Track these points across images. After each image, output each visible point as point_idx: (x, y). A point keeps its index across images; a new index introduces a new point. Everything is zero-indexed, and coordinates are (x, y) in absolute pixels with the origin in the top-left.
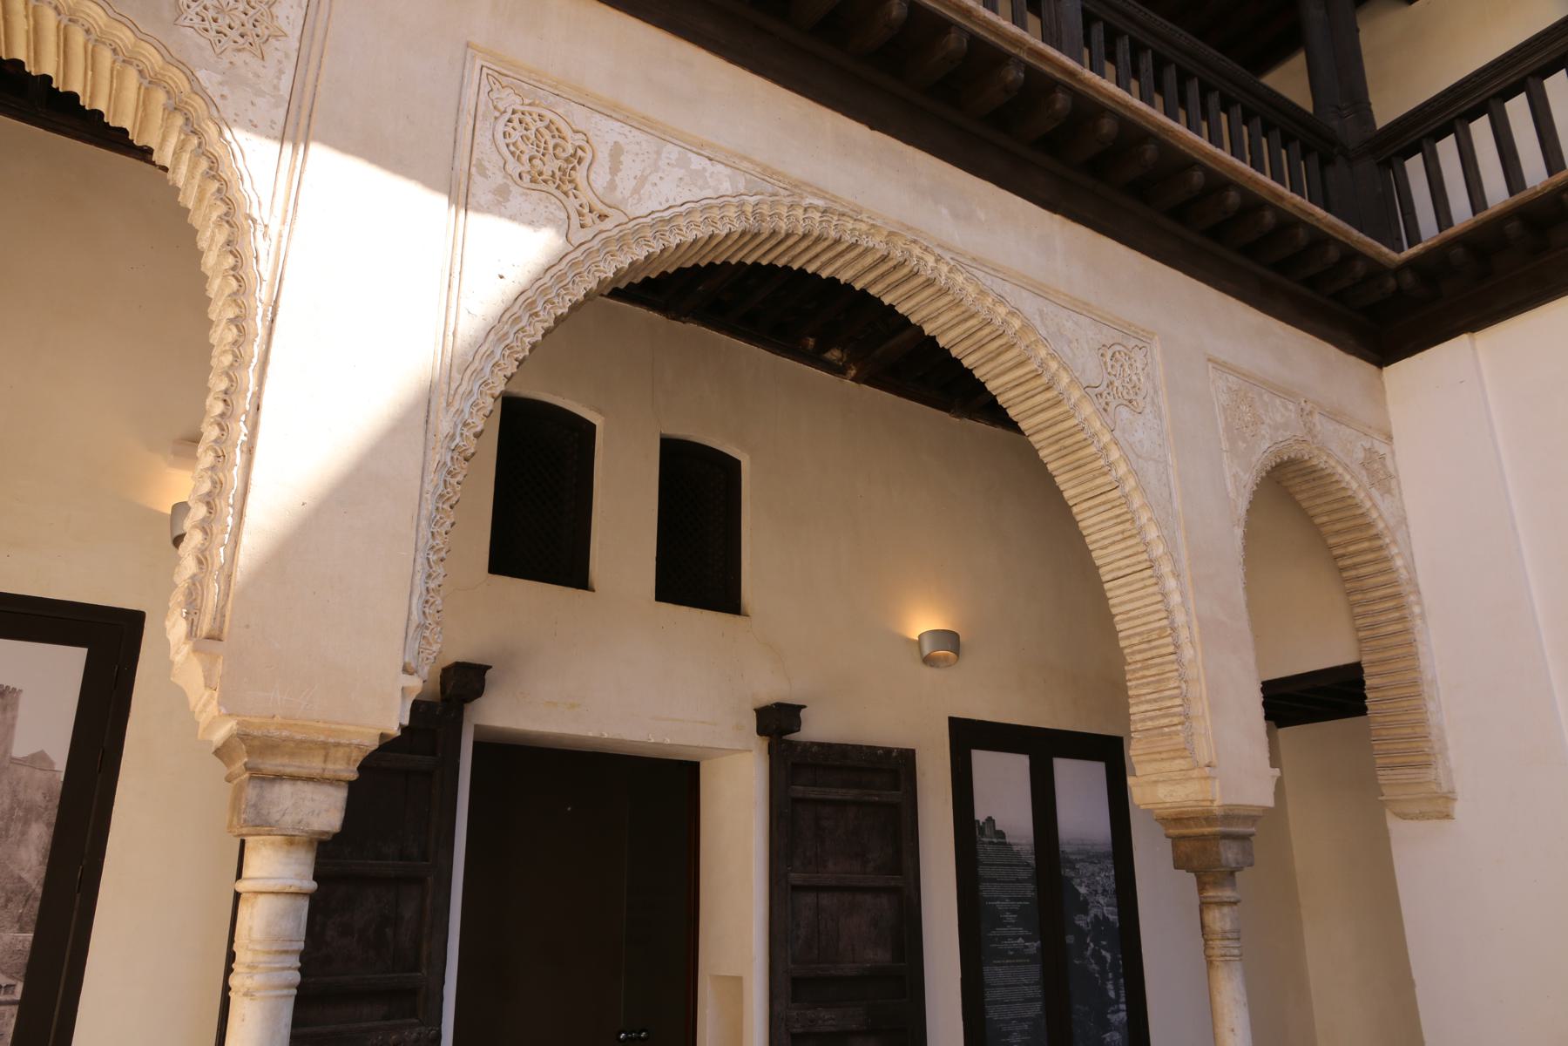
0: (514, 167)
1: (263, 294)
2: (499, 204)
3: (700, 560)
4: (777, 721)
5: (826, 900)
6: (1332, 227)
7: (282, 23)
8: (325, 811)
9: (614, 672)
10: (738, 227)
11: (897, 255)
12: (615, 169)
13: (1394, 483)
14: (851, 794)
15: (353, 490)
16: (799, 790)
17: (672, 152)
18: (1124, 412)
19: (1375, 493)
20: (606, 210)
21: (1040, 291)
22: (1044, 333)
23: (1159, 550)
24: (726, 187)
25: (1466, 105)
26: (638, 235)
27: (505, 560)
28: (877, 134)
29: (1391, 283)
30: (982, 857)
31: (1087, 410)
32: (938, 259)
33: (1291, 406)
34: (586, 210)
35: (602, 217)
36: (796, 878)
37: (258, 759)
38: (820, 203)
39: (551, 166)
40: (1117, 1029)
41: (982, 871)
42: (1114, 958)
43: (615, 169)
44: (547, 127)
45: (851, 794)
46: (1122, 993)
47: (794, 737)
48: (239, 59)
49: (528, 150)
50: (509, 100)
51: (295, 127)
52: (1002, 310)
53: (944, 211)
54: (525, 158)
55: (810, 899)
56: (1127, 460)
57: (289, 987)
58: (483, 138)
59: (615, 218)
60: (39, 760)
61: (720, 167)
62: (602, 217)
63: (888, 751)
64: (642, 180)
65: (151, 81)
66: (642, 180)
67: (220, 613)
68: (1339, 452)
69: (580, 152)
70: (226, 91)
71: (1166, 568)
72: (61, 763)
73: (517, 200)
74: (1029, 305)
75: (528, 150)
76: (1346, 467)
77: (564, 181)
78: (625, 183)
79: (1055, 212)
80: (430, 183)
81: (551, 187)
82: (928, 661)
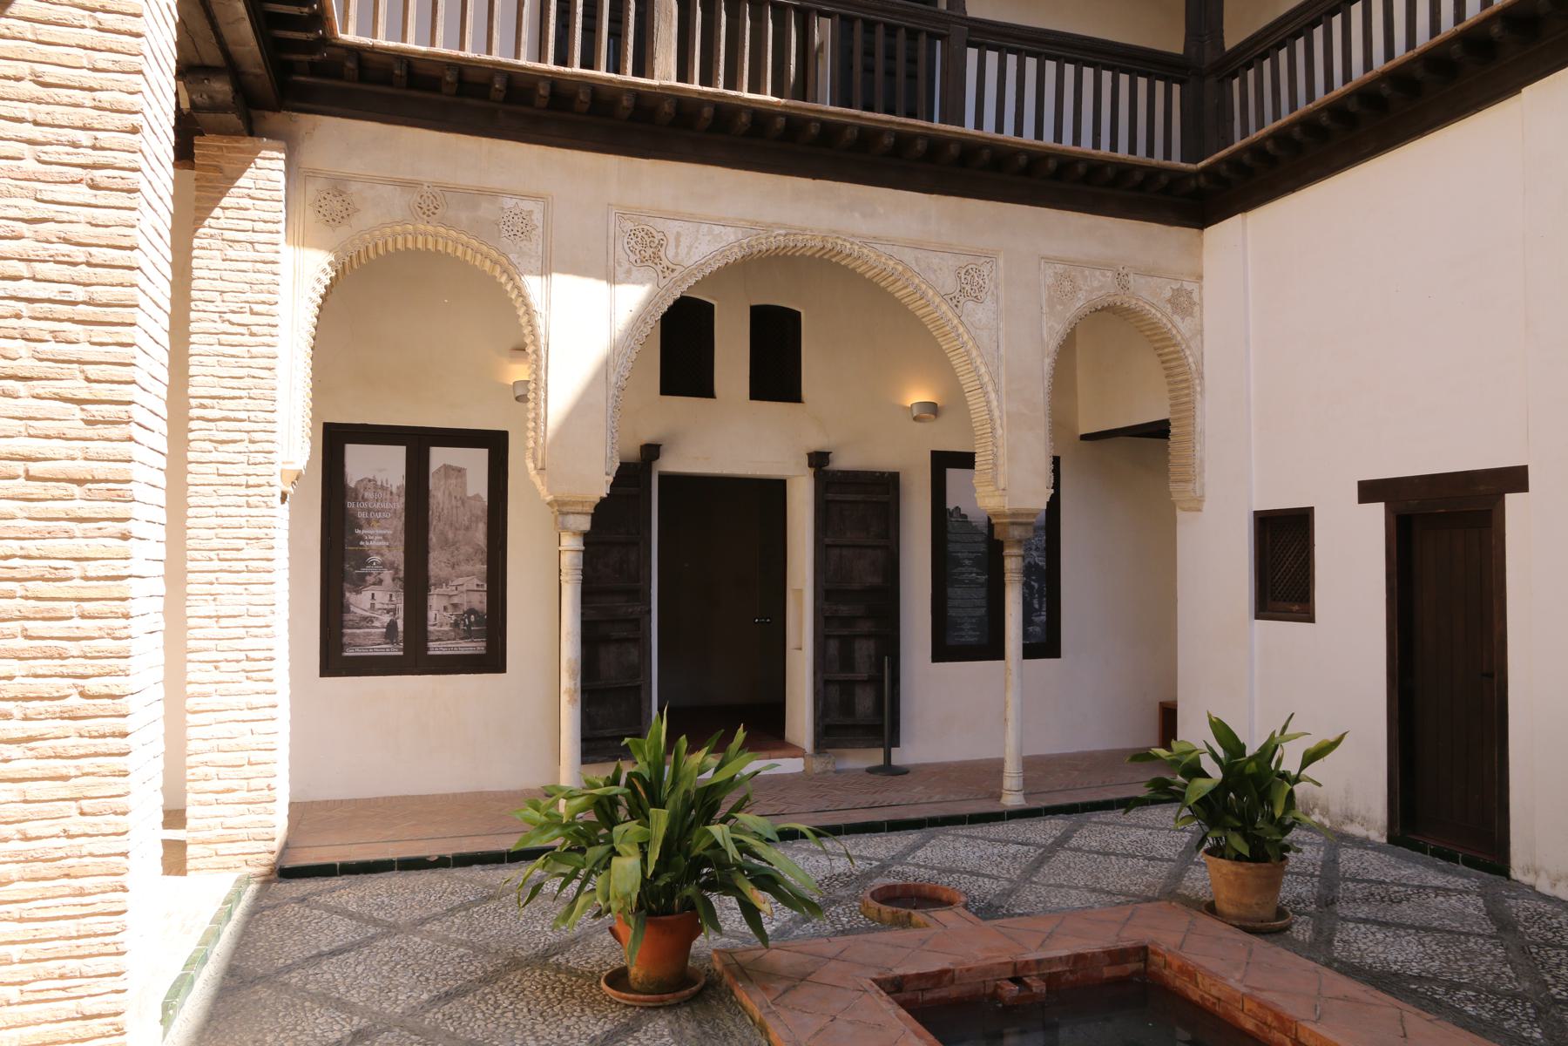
0: (633, 258)
1: (542, 340)
2: (628, 278)
3: (776, 375)
4: (818, 460)
8: (585, 524)
9: (731, 437)
10: (739, 256)
11: (829, 246)
12: (677, 246)
13: (1197, 308)
14: (859, 497)
15: (579, 409)
16: (830, 496)
17: (705, 228)
18: (970, 305)
19: (1176, 318)
21: (917, 246)
23: (986, 379)
24: (732, 238)
25: (1271, 42)
26: (691, 275)
27: (670, 386)
28: (818, 182)
29: (1193, 183)
30: (950, 528)
31: (944, 307)
33: (1109, 274)
36: (828, 541)
37: (562, 507)
39: (650, 251)
41: (949, 536)
42: (1040, 588)
43: (677, 246)
45: (859, 497)
49: (639, 247)
50: (629, 225)
51: (545, 270)
52: (891, 263)
53: (857, 215)
55: (836, 551)
56: (968, 332)
60: (477, 497)
63: (882, 474)
64: (690, 247)
65: (495, 262)
66: (690, 247)
68: (1149, 295)
71: (990, 388)
72: (486, 499)
73: (635, 273)
74: (908, 256)
75: (639, 247)
76: (1152, 305)
77: (655, 258)
78: (683, 250)
80: (599, 277)
82: (915, 419)
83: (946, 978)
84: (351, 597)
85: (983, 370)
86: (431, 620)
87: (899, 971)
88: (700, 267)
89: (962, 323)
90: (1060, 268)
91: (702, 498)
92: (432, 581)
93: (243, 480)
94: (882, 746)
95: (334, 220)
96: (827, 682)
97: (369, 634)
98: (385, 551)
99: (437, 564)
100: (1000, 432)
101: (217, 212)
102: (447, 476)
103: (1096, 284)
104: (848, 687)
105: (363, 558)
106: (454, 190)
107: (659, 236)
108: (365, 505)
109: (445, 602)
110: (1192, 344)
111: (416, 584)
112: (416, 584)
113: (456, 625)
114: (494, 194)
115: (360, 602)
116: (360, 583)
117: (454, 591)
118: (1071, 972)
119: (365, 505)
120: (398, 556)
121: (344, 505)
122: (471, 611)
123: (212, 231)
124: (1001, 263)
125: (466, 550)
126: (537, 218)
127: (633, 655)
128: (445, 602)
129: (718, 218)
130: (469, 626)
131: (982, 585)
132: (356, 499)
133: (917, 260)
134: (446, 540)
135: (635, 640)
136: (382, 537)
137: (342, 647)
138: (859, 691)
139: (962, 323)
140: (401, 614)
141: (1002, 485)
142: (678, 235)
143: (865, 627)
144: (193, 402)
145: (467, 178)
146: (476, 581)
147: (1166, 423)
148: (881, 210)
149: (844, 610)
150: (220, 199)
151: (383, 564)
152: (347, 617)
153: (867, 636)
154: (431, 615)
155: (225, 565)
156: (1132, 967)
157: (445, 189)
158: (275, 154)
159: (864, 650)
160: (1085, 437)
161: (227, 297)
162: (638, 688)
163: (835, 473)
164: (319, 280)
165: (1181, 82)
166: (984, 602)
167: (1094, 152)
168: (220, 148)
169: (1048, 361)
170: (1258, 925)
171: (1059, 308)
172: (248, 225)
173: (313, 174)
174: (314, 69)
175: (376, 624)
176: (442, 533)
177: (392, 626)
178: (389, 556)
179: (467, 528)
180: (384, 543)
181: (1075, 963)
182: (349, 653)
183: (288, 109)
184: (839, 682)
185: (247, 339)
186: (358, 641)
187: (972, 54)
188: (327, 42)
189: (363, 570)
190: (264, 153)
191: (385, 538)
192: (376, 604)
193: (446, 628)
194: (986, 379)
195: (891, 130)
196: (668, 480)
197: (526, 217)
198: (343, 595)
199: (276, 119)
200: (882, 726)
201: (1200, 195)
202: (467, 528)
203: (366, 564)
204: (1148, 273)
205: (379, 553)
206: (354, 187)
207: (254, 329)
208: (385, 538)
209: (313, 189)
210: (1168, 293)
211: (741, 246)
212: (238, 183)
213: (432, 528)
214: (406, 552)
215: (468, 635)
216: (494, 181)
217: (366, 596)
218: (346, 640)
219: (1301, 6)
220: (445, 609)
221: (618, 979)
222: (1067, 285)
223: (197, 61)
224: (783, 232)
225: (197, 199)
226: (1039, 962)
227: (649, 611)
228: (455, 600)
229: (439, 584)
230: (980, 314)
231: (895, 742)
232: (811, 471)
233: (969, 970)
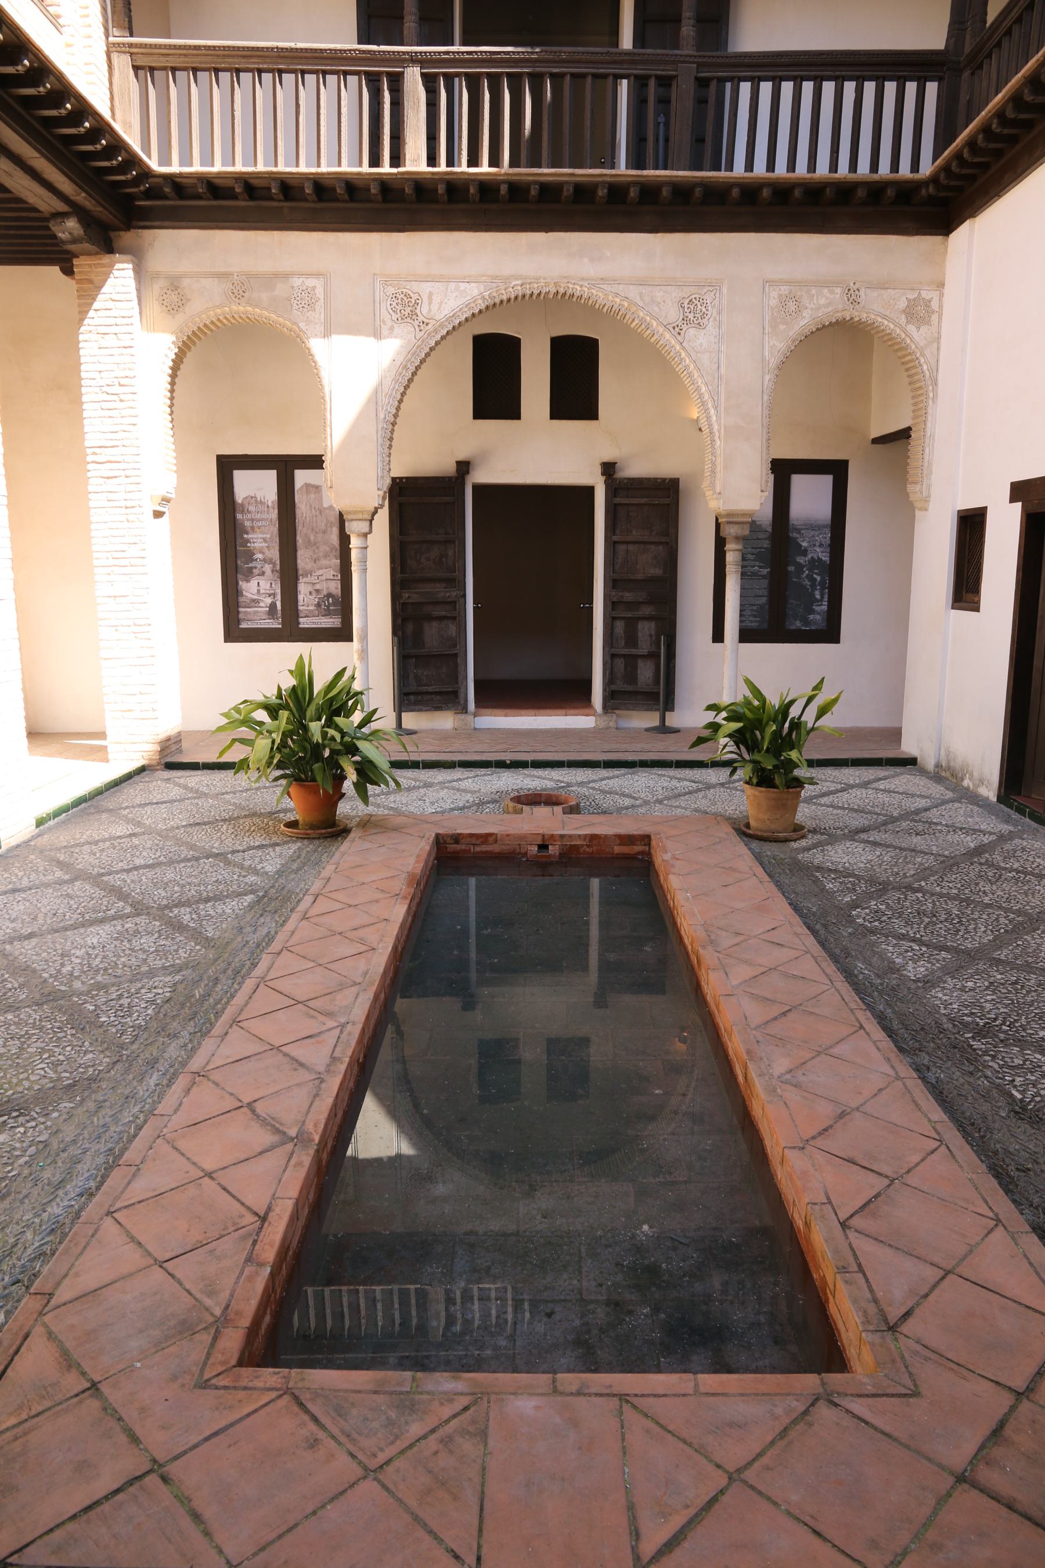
4: (608, 469)
5: (631, 547)
6: (1007, 93)
9: (538, 452)
11: (562, 291)
12: (430, 304)
13: (935, 317)
14: (643, 501)
16: (617, 500)
17: (452, 285)
18: (692, 331)
21: (642, 282)
22: (641, 304)
24: (476, 292)
26: (442, 326)
31: (668, 336)
32: (581, 286)
33: (838, 290)
36: (615, 538)
40: (819, 614)
42: (823, 581)
43: (430, 304)
46: (826, 596)
50: (391, 290)
51: (327, 334)
52: (618, 300)
53: (586, 260)
55: (623, 547)
57: (948, 761)
58: (383, 310)
59: (432, 322)
61: (473, 284)
63: (664, 480)
67: (331, 481)
68: (881, 308)
73: (397, 330)
74: (633, 293)
75: (399, 308)
77: (413, 315)
78: (435, 307)
79: (657, 232)
80: (368, 335)
81: (408, 320)
83: (491, 839)
84: (243, 584)
85: (703, 389)
86: (300, 603)
87: (458, 831)
88: (449, 319)
89: (684, 348)
90: (785, 289)
92: (300, 572)
93: (123, 504)
94: (658, 710)
95: (173, 309)
96: (613, 656)
97: (257, 612)
98: (266, 551)
99: (304, 559)
100: (718, 443)
101: (91, 313)
102: (308, 493)
103: (823, 301)
104: (631, 661)
105: (250, 556)
106: (256, 276)
108: (249, 516)
109: (310, 588)
110: (927, 352)
111: (289, 575)
112: (289, 575)
113: (318, 605)
114: (286, 276)
115: (250, 588)
116: (249, 574)
117: (316, 582)
118: (588, 846)
119: (249, 516)
120: (275, 554)
121: (235, 517)
122: (329, 595)
123: (90, 328)
124: (725, 290)
125: (324, 548)
126: (320, 292)
127: (452, 629)
128: (310, 588)
130: (328, 607)
131: (764, 577)
132: (243, 512)
133: (641, 294)
134: (309, 541)
135: (454, 618)
136: (262, 540)
137: (239, 622)
138: (640, 663)
139: (684, 348)
140: (279, 597)
141: (718, 490)
142: (431, 295)
143: (647, 610)
144: (89, 451)
145: (266, 266)
146: (333, 572)
147: (909, 429)
148: (608, 254)
150: (92, 304)
151: (264, 560)
152: (241, 599)
154: (300, 597)
155: (116, 562)
156: (638, 848)
157: (249, 276)
158: (125, 265)
159: (646, 630)
160: (876, 441)
161: (103, 374)
162: (456, 655)
163: (622, 480)
164: (166, 356)
165: (940, 80)
166: (765, 593)
167: (810, 175)
168: (90, 265)
170: (765, 834)
171: (782, 327)
172: (112, 321)
173: (157, 276)
174: (148, 194)
175: (262, 604)
176: (306, 536)
177: (273, 606)
178: (269, 554)
179: (324, 532)
180: (264, 544)
181: (590, 841)
182: (243, 625)
183: (135, 228)
184: (624, 656)
185: (118, 405)
186: (249, 617)
188: (146, 174)
189: (250, 565)
190: (118, 266)
191: (265, 540)
192: (261, 589)
193: (312, 608)
194: (706, 397)
195: (604, 182)
196: (480, 490)
197: (311, 291)
198: (237, 583)
199: (127, 237)
200: (658, 693)
201: (937, 206)
202: (324, 532)
203: (252, 560)
204: (883, 286)
205: (261, 552)
206: (186, 282)
207: (122, 397)
208: (265, 540)
209: (157, 288)
210: (903, 304)
211: (483, 298)
212: (103, 291)
213: (298, 533)
214: (281, 551)
215: (328, 613)
216: (286, 265)
217: (254, 583)
218: (241, 616)
219: (1008, 5)
220: (310, 593)
221: (292, 824)
222: (792, 306)
223: (54, 211)
224: (519, 282)
225: (79, 305)
226: (562, 836)
227: (464, 596)
228: (318, 587)
229: (305, 575)
230: (701, 340)
231: (669, 704)
232: (603, 478)
233: (508, 835)
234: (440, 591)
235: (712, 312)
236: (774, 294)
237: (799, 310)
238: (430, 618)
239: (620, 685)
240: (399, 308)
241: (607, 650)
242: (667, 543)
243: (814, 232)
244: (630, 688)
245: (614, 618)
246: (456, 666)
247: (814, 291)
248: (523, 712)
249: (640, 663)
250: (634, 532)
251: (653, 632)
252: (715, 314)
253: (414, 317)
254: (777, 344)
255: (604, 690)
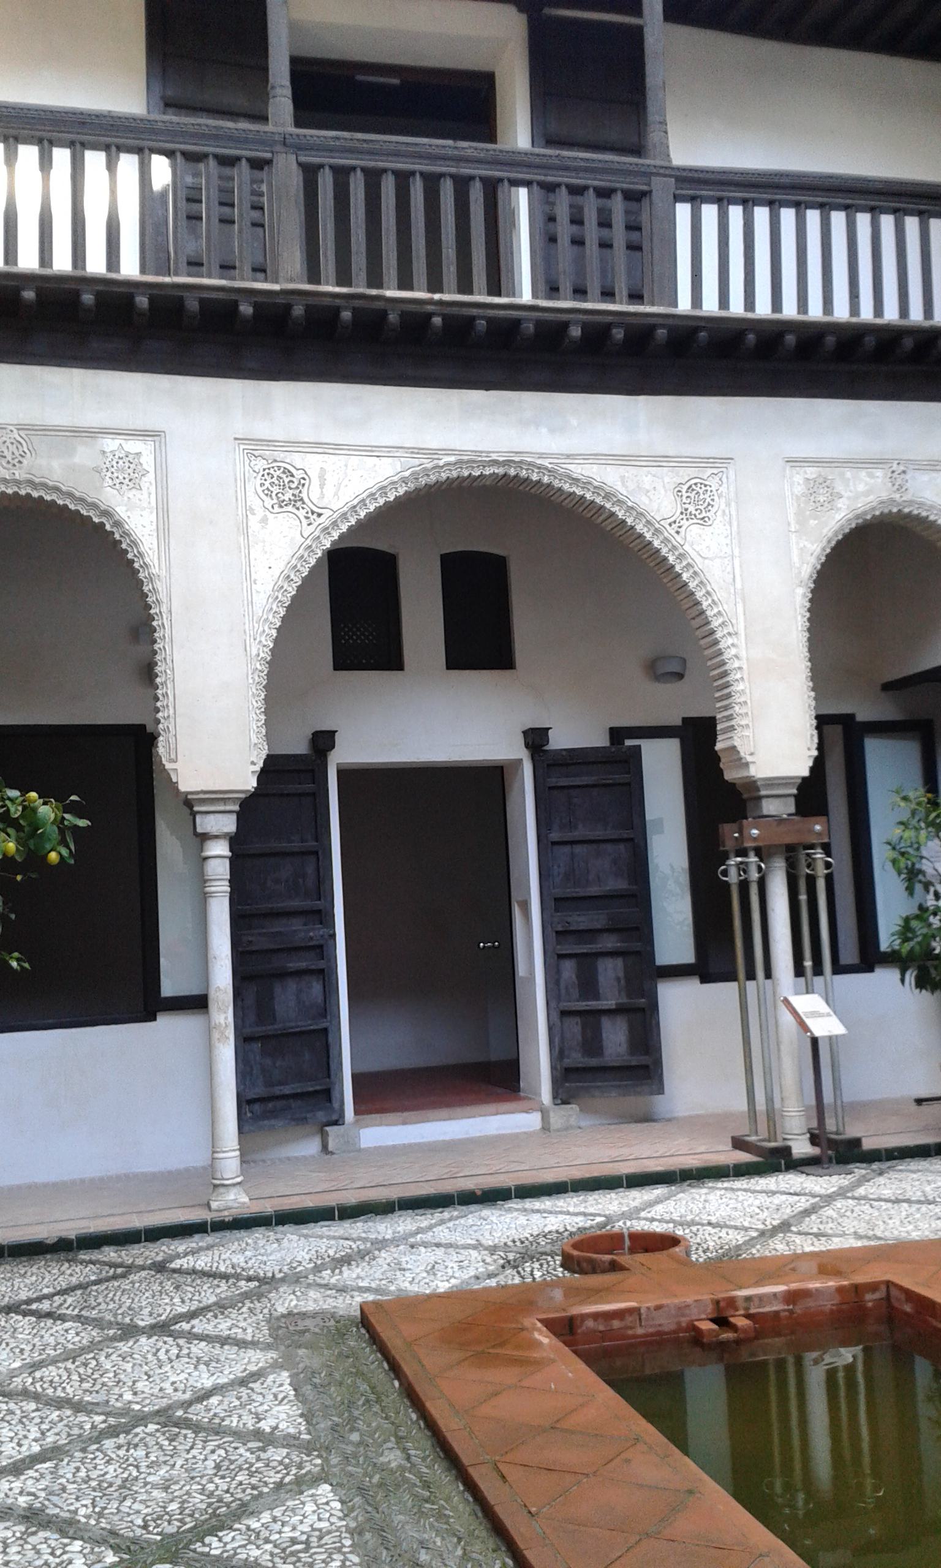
0: (268, 502)
4: (536, 739)
5: (578, 849)
7: (145, 466)
9: (433, 721)
12: (322, 486)
16: (553, 781)
18: (695, 529)
20: (320, 511)
33: (879, 473)
34: (310, 515)
35: (319, 515)
36: (555, 836)
38: (452, 459)
43: (322, 486)
44: (284, 472)
47: (546, 748)
48: (130, 494)
53: (544, 430)
54: (274, 495)
55: (566, 849)
59: (327, 513)
62: (319, 515)
64: (338, 486)
66: (338, 486)
69: (303, 481)
70: (129, 514)
77: (297, 501)
78: (329, 490)
90: (811, 472)
91: (395, 796)
103: (861, 488)
104: (591, 1018)
107: (298, 474)
114: (93, 434)
126: (147, 461)
129: (369, 445)
133: (623, 478)
138: (606, 1023)
143: (610, 942)
149: (581, 920)
153: (60, 853)
162: (325, 1030)
169: (800, 591)
171: (813, 522)
187: (683, 211)
234: (299, 930)
235: (720, 504)
236: (799, 478)
237: (835, 496)
238: (283, 975)
239: (576, 1058)
240: (275, 489)
241: (553, 1004)
242: (632, 840)
243: (838, 398)
244: (594, 1062)
245: (561, 956)
246: (327, 1047)
247: (848, 474)
248: (430, 1113)
249: (606, 1023)
250: (580, 826)
251: (621, 974)
252: (723, 506)
253: (299, 504)
254: (809, 545)
255: (553, 1068)
